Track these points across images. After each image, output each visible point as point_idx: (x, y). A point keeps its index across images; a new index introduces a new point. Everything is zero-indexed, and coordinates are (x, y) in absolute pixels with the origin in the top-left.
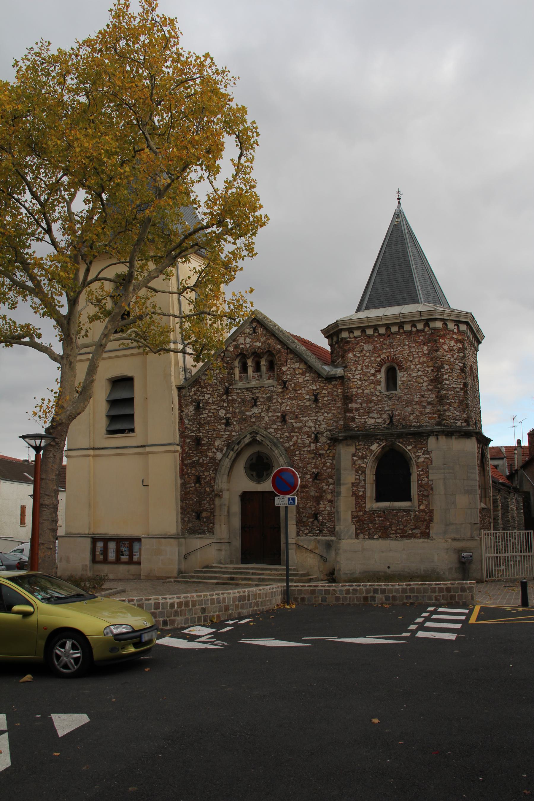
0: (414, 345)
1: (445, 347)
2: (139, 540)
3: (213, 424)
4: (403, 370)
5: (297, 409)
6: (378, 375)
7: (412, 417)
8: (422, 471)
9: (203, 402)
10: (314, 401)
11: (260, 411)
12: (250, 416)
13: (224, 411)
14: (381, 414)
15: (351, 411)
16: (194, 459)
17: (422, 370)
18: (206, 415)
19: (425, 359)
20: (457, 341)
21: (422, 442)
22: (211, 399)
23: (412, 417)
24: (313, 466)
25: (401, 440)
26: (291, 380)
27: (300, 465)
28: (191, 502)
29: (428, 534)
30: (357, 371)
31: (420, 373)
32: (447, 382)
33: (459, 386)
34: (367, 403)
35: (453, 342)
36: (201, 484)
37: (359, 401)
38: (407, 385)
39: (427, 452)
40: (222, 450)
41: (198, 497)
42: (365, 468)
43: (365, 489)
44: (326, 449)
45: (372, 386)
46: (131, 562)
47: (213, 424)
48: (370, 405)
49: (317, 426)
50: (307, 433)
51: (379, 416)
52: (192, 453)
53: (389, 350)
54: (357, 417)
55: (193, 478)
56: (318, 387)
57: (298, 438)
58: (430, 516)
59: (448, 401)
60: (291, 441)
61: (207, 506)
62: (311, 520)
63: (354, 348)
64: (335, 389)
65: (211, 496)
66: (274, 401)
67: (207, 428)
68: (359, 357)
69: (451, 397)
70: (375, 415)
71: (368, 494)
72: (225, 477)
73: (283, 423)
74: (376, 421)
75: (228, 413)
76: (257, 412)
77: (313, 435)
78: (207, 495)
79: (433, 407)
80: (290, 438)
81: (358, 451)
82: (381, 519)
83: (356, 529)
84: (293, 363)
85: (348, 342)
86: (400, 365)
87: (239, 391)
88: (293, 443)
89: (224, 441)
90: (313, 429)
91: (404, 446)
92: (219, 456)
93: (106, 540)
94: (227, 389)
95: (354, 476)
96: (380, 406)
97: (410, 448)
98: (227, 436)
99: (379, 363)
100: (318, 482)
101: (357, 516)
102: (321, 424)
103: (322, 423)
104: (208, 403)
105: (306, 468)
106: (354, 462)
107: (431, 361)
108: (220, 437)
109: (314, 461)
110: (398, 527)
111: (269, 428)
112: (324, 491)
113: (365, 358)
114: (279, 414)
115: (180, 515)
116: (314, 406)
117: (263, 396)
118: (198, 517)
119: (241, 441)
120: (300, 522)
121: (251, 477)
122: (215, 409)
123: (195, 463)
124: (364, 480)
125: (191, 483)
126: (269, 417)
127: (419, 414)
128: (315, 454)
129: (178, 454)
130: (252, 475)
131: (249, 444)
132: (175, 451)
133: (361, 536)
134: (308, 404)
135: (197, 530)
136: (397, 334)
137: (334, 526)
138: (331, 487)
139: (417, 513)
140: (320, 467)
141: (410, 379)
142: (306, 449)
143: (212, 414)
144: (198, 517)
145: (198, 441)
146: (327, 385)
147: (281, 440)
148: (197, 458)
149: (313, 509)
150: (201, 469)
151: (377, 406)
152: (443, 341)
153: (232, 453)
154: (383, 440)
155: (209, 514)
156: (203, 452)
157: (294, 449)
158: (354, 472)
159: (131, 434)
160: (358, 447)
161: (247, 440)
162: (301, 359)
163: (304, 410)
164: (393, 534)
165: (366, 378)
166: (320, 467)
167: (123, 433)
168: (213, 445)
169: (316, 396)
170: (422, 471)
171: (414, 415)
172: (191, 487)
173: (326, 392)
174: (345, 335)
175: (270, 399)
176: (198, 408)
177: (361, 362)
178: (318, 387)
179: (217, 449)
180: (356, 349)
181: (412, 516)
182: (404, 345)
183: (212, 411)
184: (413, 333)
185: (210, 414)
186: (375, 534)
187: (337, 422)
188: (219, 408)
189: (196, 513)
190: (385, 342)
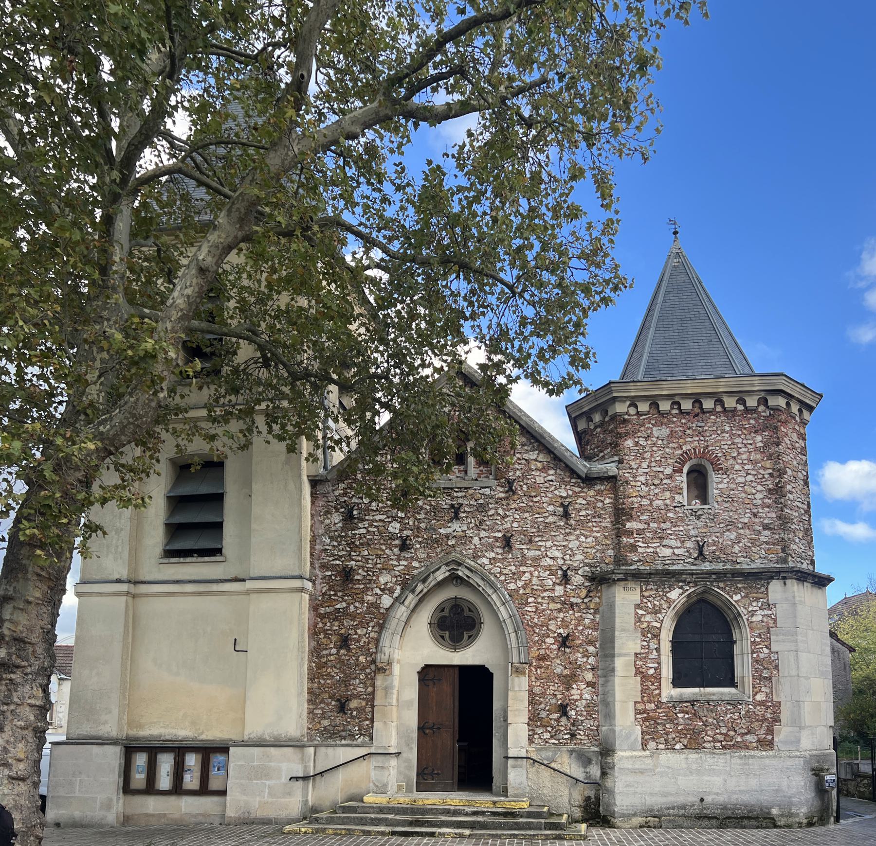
0: (740, 433)
2: (224, 749)
3: (377, 546)
5: (532, 526)
6: (678, 478)
7: (737, 549)
8: (760, 636)
9: (359, 509)
11: (465, 528)
12: (447, 536)
13: (398, 525)
14: (683, 542)
15: (629, 533)
16: (338, 606)
17: (754, 473)
18: (364, 531)
19: (759, 457)
21: (760, 589)
23: (737, 549)
24: (559, 623)
25: (722, 585)
26: (523, 478)
27: (536, 620)
28: (328, 681)
30: (639, 470)
31: (750, 478)
32: (791, 497)
34: (659, 523)
36: (349, 649)
40: (391, 591)
41: (343, 672)
42: (660, 629)
43: (659, 664)
44: (583, 596)
45: (668, 494)
46: (204, 790)
47: (377, 546)
48: (663, 526)
49: (568, 557)
50: (548, 568)
51: (679, 545)
52: (335, 595)
53: (697, 438)
54: (640, 544)
55: (334, 638)
56: (570, 493)
57: (532, 575)
61: (359, 689)
62: (556, 716)
63: (635, 432)
64: (599, 498)
65: (368, 671)
66: (491, 512)
67: (366, 553)
68: (644, 447)
70: (674, 543)
73: (507, 549)
74: (674, 553)
75: (406, 529)
76: (460, 530)
77: (560, 572)
78: (360, 670)
81: (645, 600)
82: (687, 716)
83: (643, 733)
84: (527, 452)
85: (625, 421)
88: (523, 583)
89: (396, 577)
90: (561, 562)
91: (728, 594)
92: (386, 601)
93: (154, 750)
95: (639, 641)
96: (681, 528)
97: (737, 597)
100: (568, 650)
101: (645, 711)
104: (368, 510)
105: (547, 626)
106: (639, 619)
108: (388, 569)
109: (562, 615)
110: (718, 731)
111: (479, 557)
112: (580, 667)
113: (655, 449)
114: (500, 535)
116: (562, 524)
117: (472, 503)
118: (342, 708)
119: (428, 576)
120: (534, 720)
121: (440, 639)
122: (380, 520)
123: (339, 612)
124: (658, 650)
125: (331, 648)
126: (480, 539)
127: (750, 545)
128: (564, 603)
130: (443, 637)
131: (440, 584)
132: (303, 590)
133: (652, 745)
134: (551, 519)
135: (339, 732)
136: (712, 412)
138: (591, 660)
141: (733, 486)
142: (545, 594)
143: (375, 529)
144: (342, 708)
145: (347, 575)
146: (585, 490)
147: (503, 578)
148: (344, 605)
149: (559, 697)
150: (352, 623)
151: (677, 528)
153: (411, 596)
154: (689, 582)
155: (364, 703)
158: (639, 635)
160: (646, 594)
161: (441, 575)
163: (544, 529)
164: (709, 742)
165: (657, 482)
169: (565, 508)
170: (760, 636)
171: (741, 545)
172: (331, 655)
173: (584, 502)
174: (620, 408)
175: (482, 509)
176: (349, 518)
177: (647, 455)
178: (570, 493)
180: (639, 434)
182: (723, 431)
183: (375, 524)
186: (677, 742)
187: (602, 551)
188: (390, 520)
189: (338, 700)
190: (689, 425)
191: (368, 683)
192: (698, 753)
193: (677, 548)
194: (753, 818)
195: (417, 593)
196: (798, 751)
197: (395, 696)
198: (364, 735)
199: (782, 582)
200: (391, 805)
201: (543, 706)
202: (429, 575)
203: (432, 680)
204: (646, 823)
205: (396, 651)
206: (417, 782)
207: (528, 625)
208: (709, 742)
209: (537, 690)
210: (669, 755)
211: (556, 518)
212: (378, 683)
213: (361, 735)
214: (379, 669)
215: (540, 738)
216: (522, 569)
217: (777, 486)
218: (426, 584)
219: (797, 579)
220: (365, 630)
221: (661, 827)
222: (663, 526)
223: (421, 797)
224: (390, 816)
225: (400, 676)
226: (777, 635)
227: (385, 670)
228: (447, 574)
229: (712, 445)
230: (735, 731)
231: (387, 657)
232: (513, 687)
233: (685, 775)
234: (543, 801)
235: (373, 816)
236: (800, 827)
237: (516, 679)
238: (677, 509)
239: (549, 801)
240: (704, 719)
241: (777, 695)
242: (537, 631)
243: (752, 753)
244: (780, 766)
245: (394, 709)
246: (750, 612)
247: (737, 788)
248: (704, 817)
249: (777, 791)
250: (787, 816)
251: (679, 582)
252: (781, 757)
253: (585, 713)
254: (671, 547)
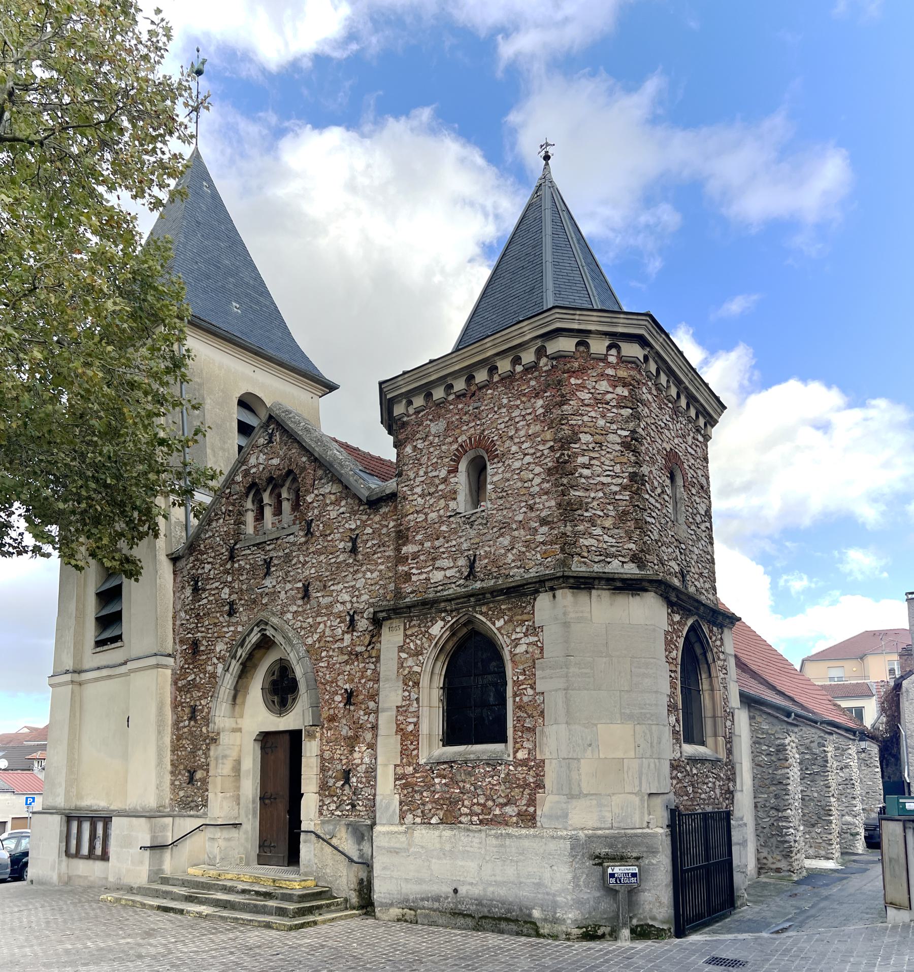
0: (518, 402)
1: (584, 395)
3: (214, 615)
4: (496, 460)
6: (452, 480)
7: (510, 556)
8: (524, 673)
10: (351, 551)
11: (274, 583)
14: (455, 560)
16: (189, 679)
17: (532, 451)
18: (205, 601)
19: (538, 428)
20: (616, 382)
21: (525, 607)
22: (212, 572)
23: (510, 556)
25: (484, 609)
26: (320, 515)
28: (183, 753)
29: (533, 817)
31: (528, 459)
32: (586, 472)
33: (619, 481)
34: (432, 542)
35: (605, 383)
36: (196, 721)
37: (419, 537)
38: (503, 491)
39: (534, 630)
41: (193, 744)
45: (442, 503)
48: (437, 543)
49: (355, 599)
52: (188, 668)
53: (473, 424)
54: (414, 571)
56: (358, 523)
58: (537, 775)
59: (586, 514)
61: (202, 760)
68: (421, 450)
69: (595, 503)
70: (446, 563)
71: (424, 728)
77: (348, 618)
79: (552, 528)
80: (313, 627)
81: (408, 641)
82: (444, 781)
83: (401, 803)
86: (490, 449)
87: (248, 552)
89: (227, 644)
91: (490, 620)
93: (80, 820)
94: (232, 550)
95: (400, 692)
96: (454, 543)
98: (230, 633)
99: (455, 455)
100: (352, 708)
101: (403, 776)
102: (361, 595)
103: (363, 592)
106: (401, 666)
107: (549, 429)
110: (475, 801)
113: (431, 450)
115: (168, 778)
117: (280, 554)
120: (324, 788)
122: (217, 588)
124: (417, 699)
127: (524, 549)
129: (169, 672)
137: (375, 795)
139: (511, 768)
140: (356, 680)
141: (508, 475)
148: (193, 676)
149: (344, 761)
152: (579, 382)
153: (234, 662)
154: (452, 611)
156: (201, 665)
157: (319, 648)
158: (400, 684)
159: (119, 644)
162: (336, 479)
164: (466, 815)
165: (432, 490)
166: (356, 680)
167: (117, 641)
168: (213, 651)
169: (354, 541)
170: (524, 673)
171: (514, 551)
175: (288, 558)
179: (218, 659)
180: (418, 436)
181: (502, 776)
183: (213, 592)
184: (517, 377)
185: (211, 598)
186: (434, 815)
188: (221, 586)
192: (452, 829)
193: (449, 568)
194: (512, 921)
196: (566, 829)
199: (551, 594)
202: (245, 638)
203: (270, 747)
204: (403, 916)
208: (466, 815)
209: (327, 755)
210: (424, 831)
211: (346, 555)
212: (212, 753)
215: (328, 809)
217: (558, 462)
219: (571, 588)
221: (417, 923)
222: (437, 543)
226: (543, 670)
229: (488, 428)
230: (494, 801)
233: (439, 858)
236: (568, 939)
237: (308, 743)
238: (452, 519)
239: (331, 882)
240: (461, 784)
241: (541, 752)
243: (510, 830)
244: (542, 851)
246: (512, 640)
247: (493, 878)
248: (460, 914)
249: (539, 885)
250: (551, 922)
251: (441, 612)
252: (542, 837)
253: (364, 780)
254: (443, 569)
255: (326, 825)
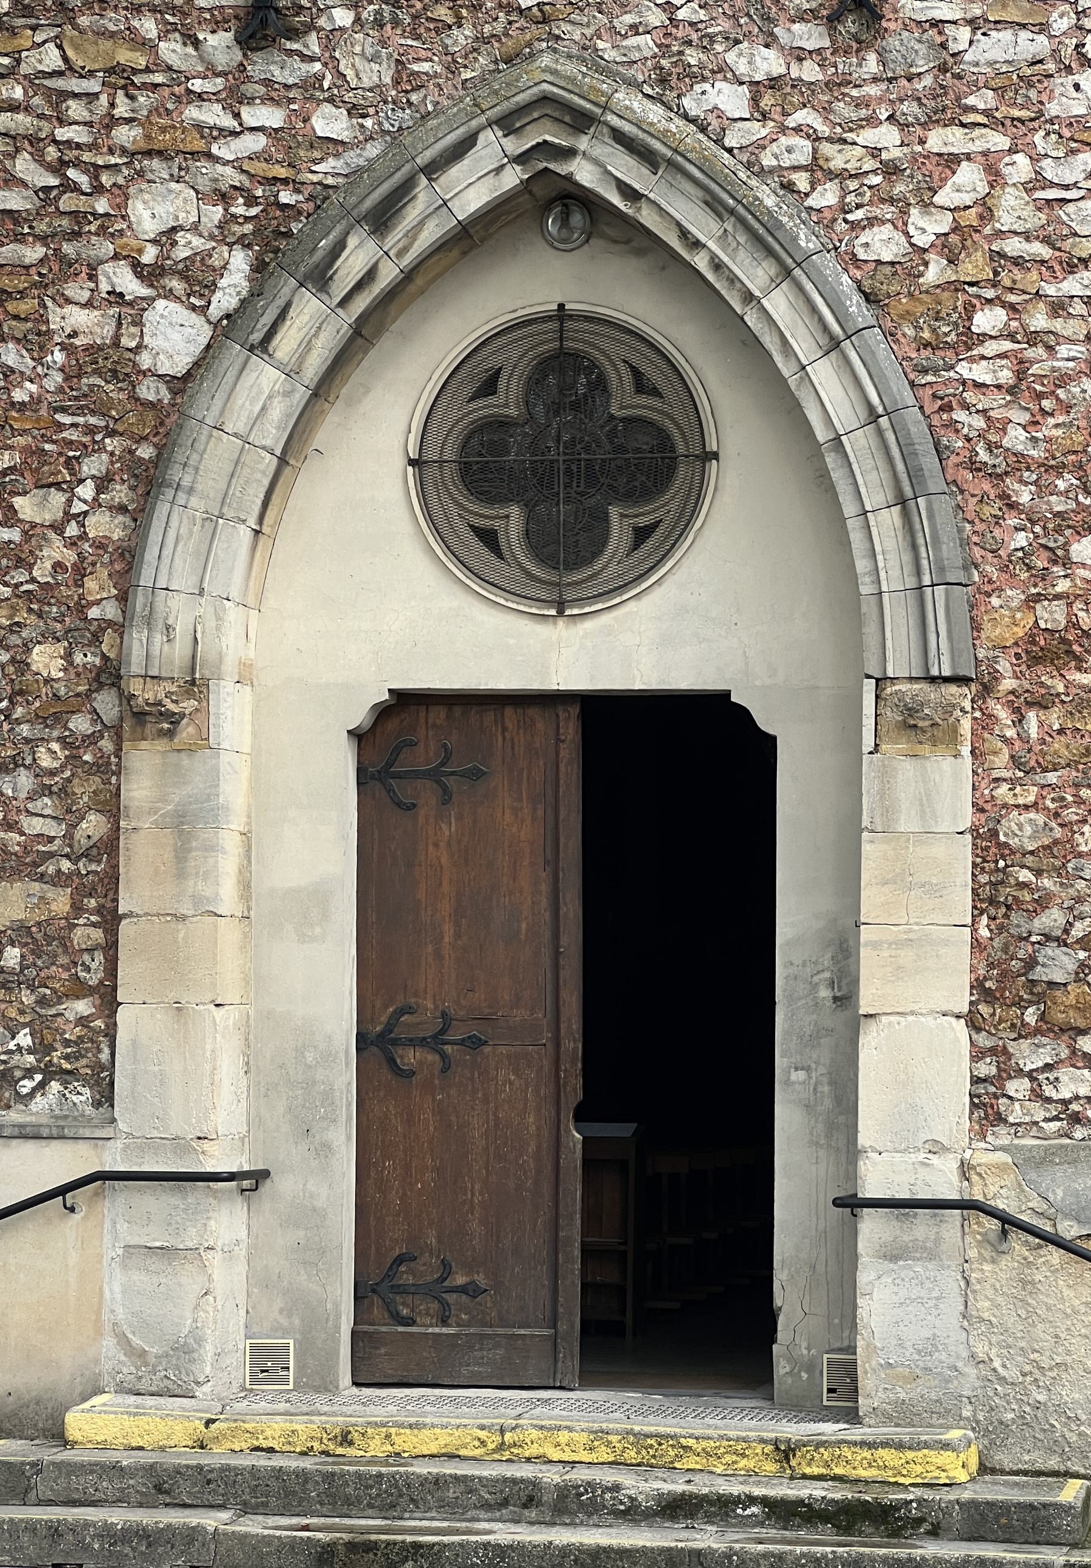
27: (1016, 438)
57: (994, 175)
60: (927, 206)
61: (35, 826)
65: (80, 724)
67: (51, 58)
72: (244, 534)
73: (850, 25)
78: (38, 718)
88: (943, 223)
89: (224, 198)
98: (255, 143)
111: (694, 76)
119: (403, 192)
130: (489, 538)
147: (826, 196)
155: (60, 902)
179: (148, 274)
191: (84, 790)
195: (342, 285)
197: (228, 864)
198: (67, 1076)
200: (217, 1457)
201: (1053, 919)
203: (434, 775)
205: (233, 613)
206: (354, 1333)
207: (974, 466)
213: (50, 1073)
214: (140, 717)
215: (1037, 1095)
216: (939, 140)
218: (395, 237)
220: (58, 498)
223: (378, 1413)
224: (212, 1520)
225: (256, 754)
227: (175, 719)
228: (512, 177)
231: (180, 650)
232: (889, 811)
234: (1055, 1446)
235: (117, 1517)
237: (906, 769)
242: (1025, 496)
245: (229, 934)
255: (1059, 1172)
